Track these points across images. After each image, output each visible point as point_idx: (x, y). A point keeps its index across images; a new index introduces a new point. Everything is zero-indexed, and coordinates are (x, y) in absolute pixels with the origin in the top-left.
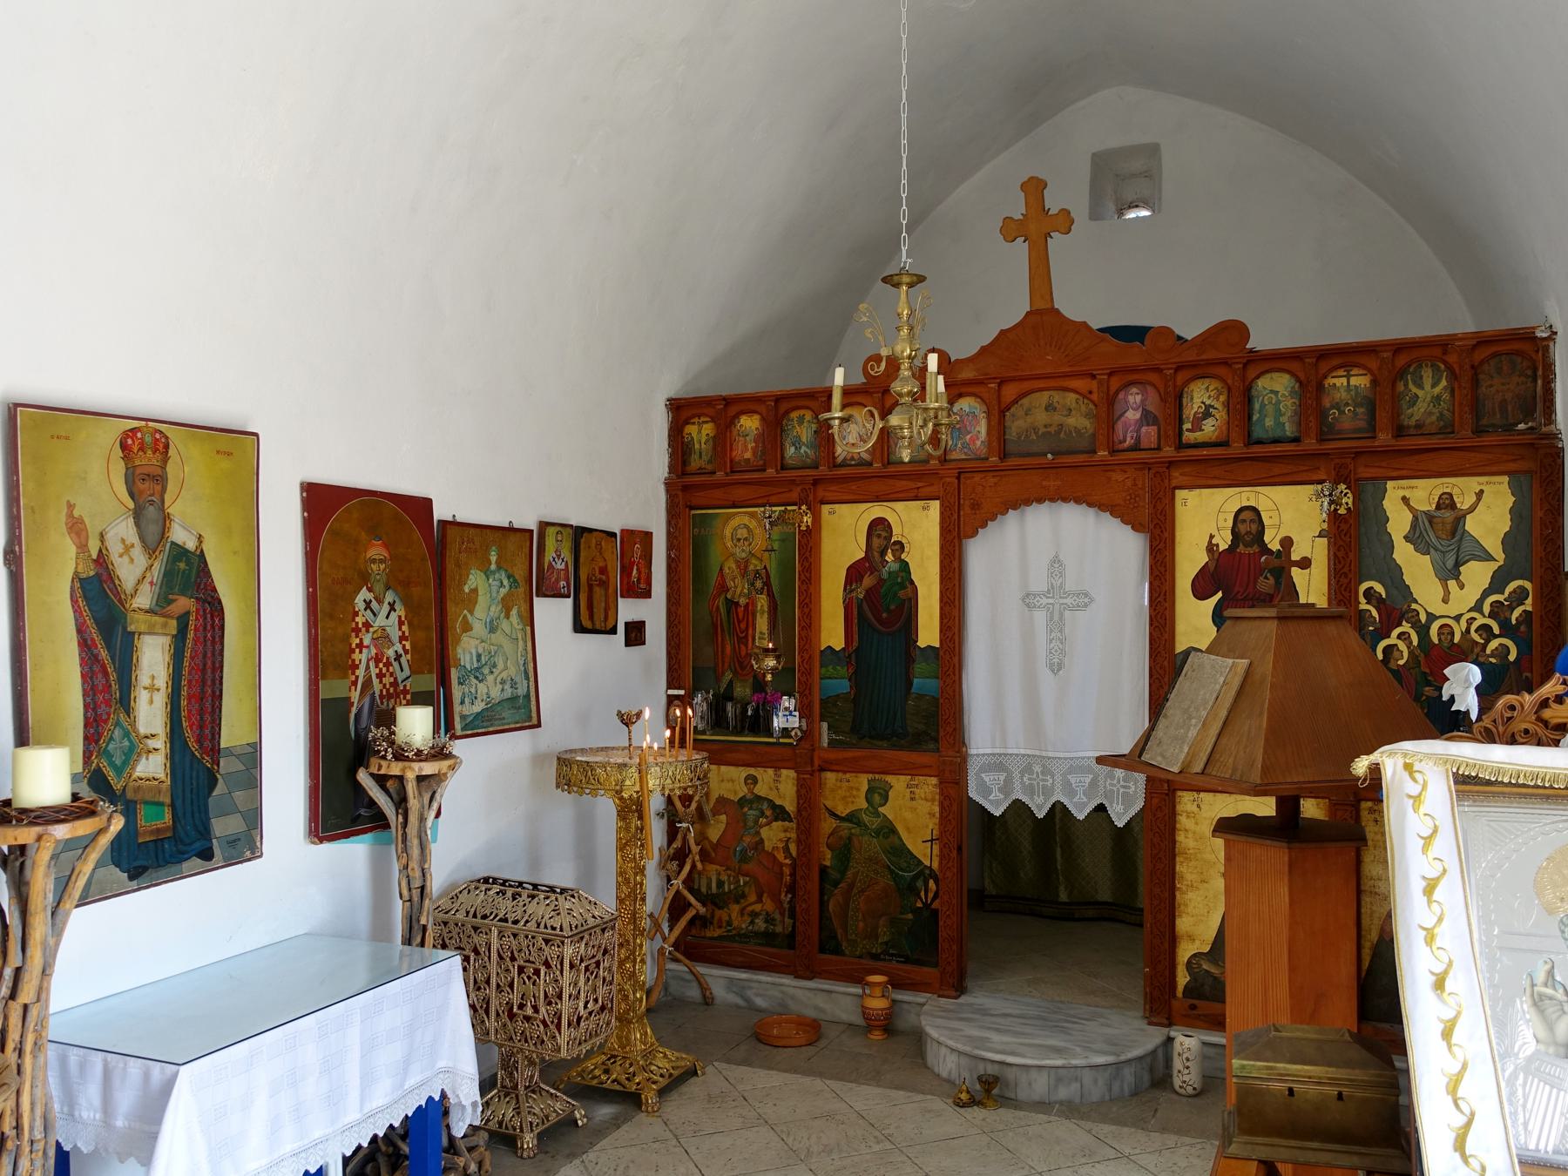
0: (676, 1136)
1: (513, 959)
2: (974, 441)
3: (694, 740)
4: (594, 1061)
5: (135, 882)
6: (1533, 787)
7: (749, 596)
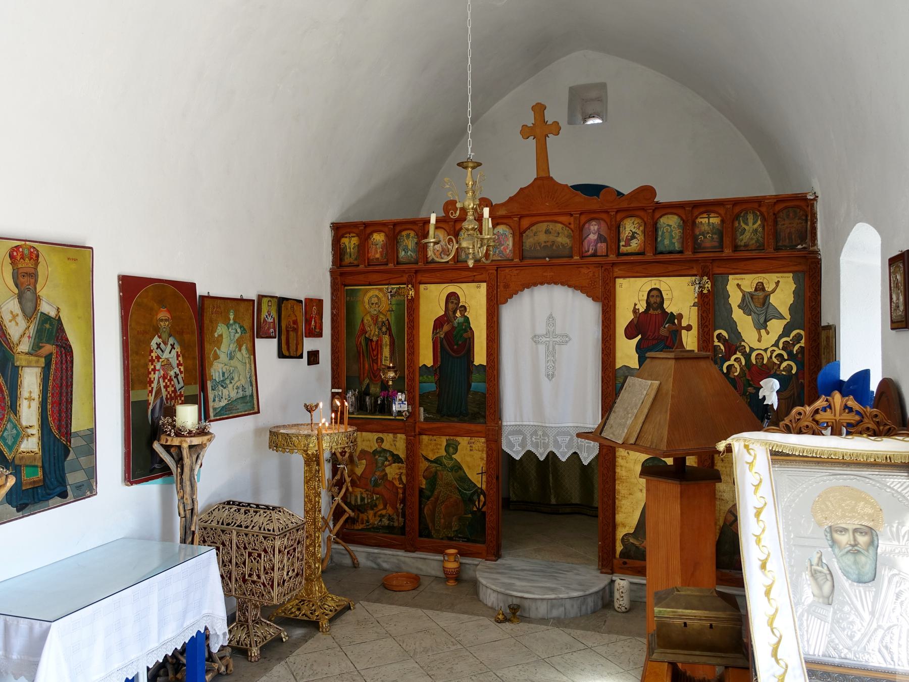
0: (340, 646)
1: (245, 548)
2: (505, 250)
3: (349, 418)
4: (291, 604)
5: (21, 513)
6: (811, 457)
7: (378, 336)
